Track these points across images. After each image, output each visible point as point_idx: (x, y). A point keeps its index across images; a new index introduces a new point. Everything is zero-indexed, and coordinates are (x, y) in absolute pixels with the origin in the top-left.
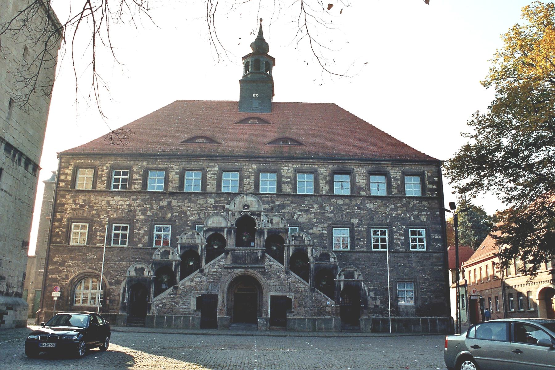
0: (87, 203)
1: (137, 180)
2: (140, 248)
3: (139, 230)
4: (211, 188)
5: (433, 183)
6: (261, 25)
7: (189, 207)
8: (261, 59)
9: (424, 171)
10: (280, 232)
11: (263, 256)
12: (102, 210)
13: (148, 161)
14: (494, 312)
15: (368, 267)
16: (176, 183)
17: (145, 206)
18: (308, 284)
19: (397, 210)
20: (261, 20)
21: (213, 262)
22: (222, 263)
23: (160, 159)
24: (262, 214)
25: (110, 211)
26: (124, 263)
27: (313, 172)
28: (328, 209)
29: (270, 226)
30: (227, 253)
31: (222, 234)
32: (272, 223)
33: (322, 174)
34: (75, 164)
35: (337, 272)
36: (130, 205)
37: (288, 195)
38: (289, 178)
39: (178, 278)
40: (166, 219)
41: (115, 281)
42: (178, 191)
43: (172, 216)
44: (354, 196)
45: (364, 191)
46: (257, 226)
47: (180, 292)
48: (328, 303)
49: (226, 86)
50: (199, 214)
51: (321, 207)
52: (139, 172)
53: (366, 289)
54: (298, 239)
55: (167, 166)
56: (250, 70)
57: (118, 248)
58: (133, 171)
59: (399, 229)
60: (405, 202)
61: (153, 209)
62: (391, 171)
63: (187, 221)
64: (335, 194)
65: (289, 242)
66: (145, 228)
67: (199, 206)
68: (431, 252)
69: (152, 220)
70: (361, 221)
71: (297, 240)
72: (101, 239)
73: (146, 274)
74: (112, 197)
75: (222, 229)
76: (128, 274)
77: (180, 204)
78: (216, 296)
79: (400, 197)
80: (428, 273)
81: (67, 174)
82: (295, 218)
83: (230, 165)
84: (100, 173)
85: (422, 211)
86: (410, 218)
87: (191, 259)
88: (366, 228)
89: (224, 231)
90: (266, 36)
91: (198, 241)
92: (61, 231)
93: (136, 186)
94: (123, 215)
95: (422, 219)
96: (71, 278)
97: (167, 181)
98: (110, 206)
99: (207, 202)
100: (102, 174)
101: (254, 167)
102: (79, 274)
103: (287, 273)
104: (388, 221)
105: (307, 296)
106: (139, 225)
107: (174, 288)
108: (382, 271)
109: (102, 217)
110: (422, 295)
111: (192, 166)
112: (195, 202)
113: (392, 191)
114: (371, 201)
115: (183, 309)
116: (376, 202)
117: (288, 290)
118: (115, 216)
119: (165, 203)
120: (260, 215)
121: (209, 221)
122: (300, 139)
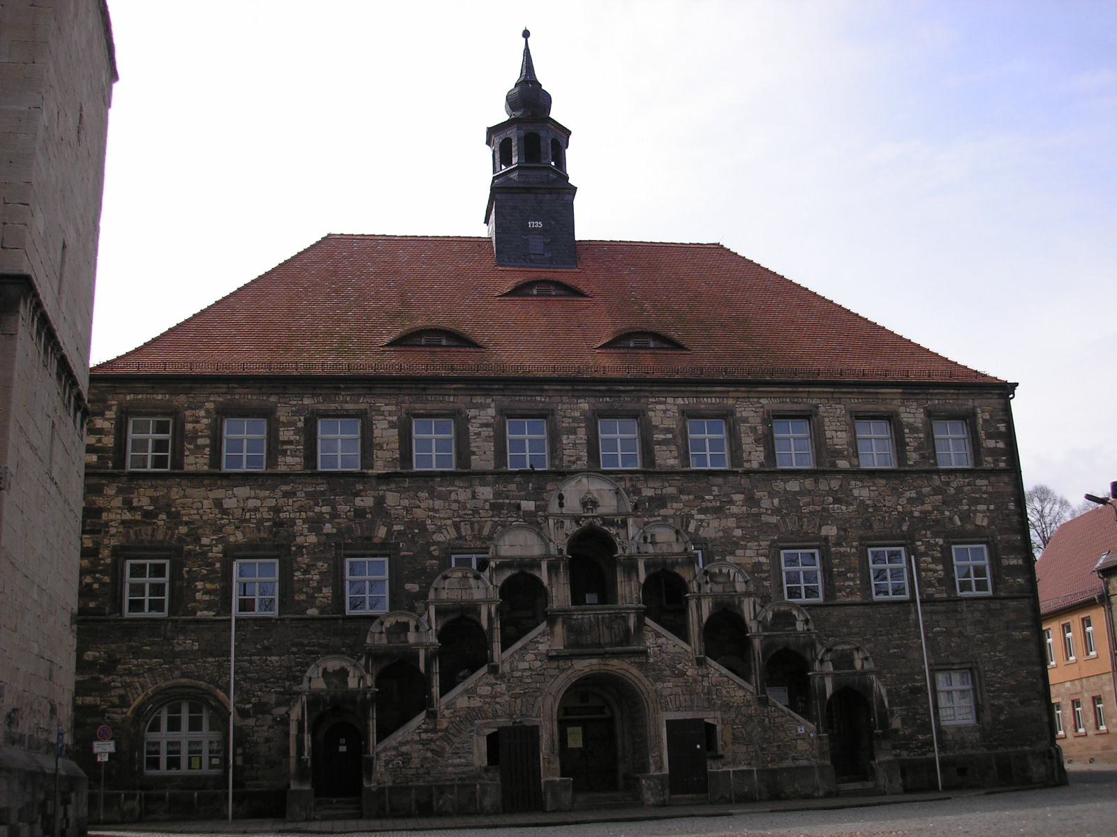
0: (163, 506)
1: (290, 442)
2: (313, 619)
3: (306, 572)
4: (482, 459)
5: (996, 435)
6: (527, 52)
7: (430, 510)
8: (542, 134)
9: (974, 408)
10: (675, 564)
11: (640, 624)
12: (205, 522)
13: (313, 395)
14: (1091, 733)
15: (869, 641)
16: (392, 450)
17: (317, 509)
18: (751, 688)
19: (923, 503)
20: (526, 34)
21: (519, 644)
22: (543, 648)
23: (346, 389)
24: (630, 521)
25: (225, 525)
26: (274, 658)
27: (726, 415)
28: (766, 503)
29: (650, 549)
30: (552, 622)
31: (537, 574)
32: (654, 543)
33: (746, 420)
34: (120, 406)
35: (816, 655)
36: (277, 510)
37: (668, 474)
38: (668, 430)
39: (436, 690)
40: (375, 540)
41: (255, 705)
42: (399, 470)
43: (390, 532)
44: (824, 472)
45: (845, 458)
46: (620, 551)
47: (445, 725)
48: (801, 730)
49: (454, 200)
50: (457, 526)
51: (751, 501)
52: (293, 424)
53: (883, 692)
54: (720, 579)
55: (363, 406)
56: (515, 160)
57: (255, 620)
58: (278, 420)
59: (930, 547)
60: (937, 483)
61: (339, 516)
62: (902, 409)
63: (429, 544)
64: (779, 467)
65: (699, 586)
66: (322, 566)
67: (455, 506)
68: (1004, 598)
69: (338, 546)
70: (845, 530)
71: (717, 583)
72: (207, 597)
73: (352, 683)
74: (226, 488)
75: (535, 563)
76: (305, 686)
77: (406, 502)
78: (533, 732)
79: (927, 472)
80: (1000, 648)
81: (100, 431)
82: (691, 528)
83: (523, 401)
84: (189, 426)
85: (977, 501)
86: (951, 519)
87: (463, 645)
88: (856, 548)
89: (539, 567)
90: (541, 75)
91: (478, 595)
92: (97, 580)
93: (289, 460)
94: (262, 535)
95: (978, 522)
96: (135, 704)
97: (368, 445)
98: (225, 512)
99: (474, 497)
100: (195, 431)
101: (584, 405)
102: (156, 693)
103: (700, 662)
104: (905, 528)
105: (751, 716)
106: (304, 560)
107: (428, 716)
108: (898, 647)
109: (205, 541)
110: (993, 698)
111: (429, 406)
112: (445, 497)
113: (907, 459)
114: (861, 481)
115: (455, 766)
116: (874, 485)
117: (706, 704)
118: (239, 536)
119: (366, 501)
120: (624, 524)
121: (501, 543)
122: (674, 335)
